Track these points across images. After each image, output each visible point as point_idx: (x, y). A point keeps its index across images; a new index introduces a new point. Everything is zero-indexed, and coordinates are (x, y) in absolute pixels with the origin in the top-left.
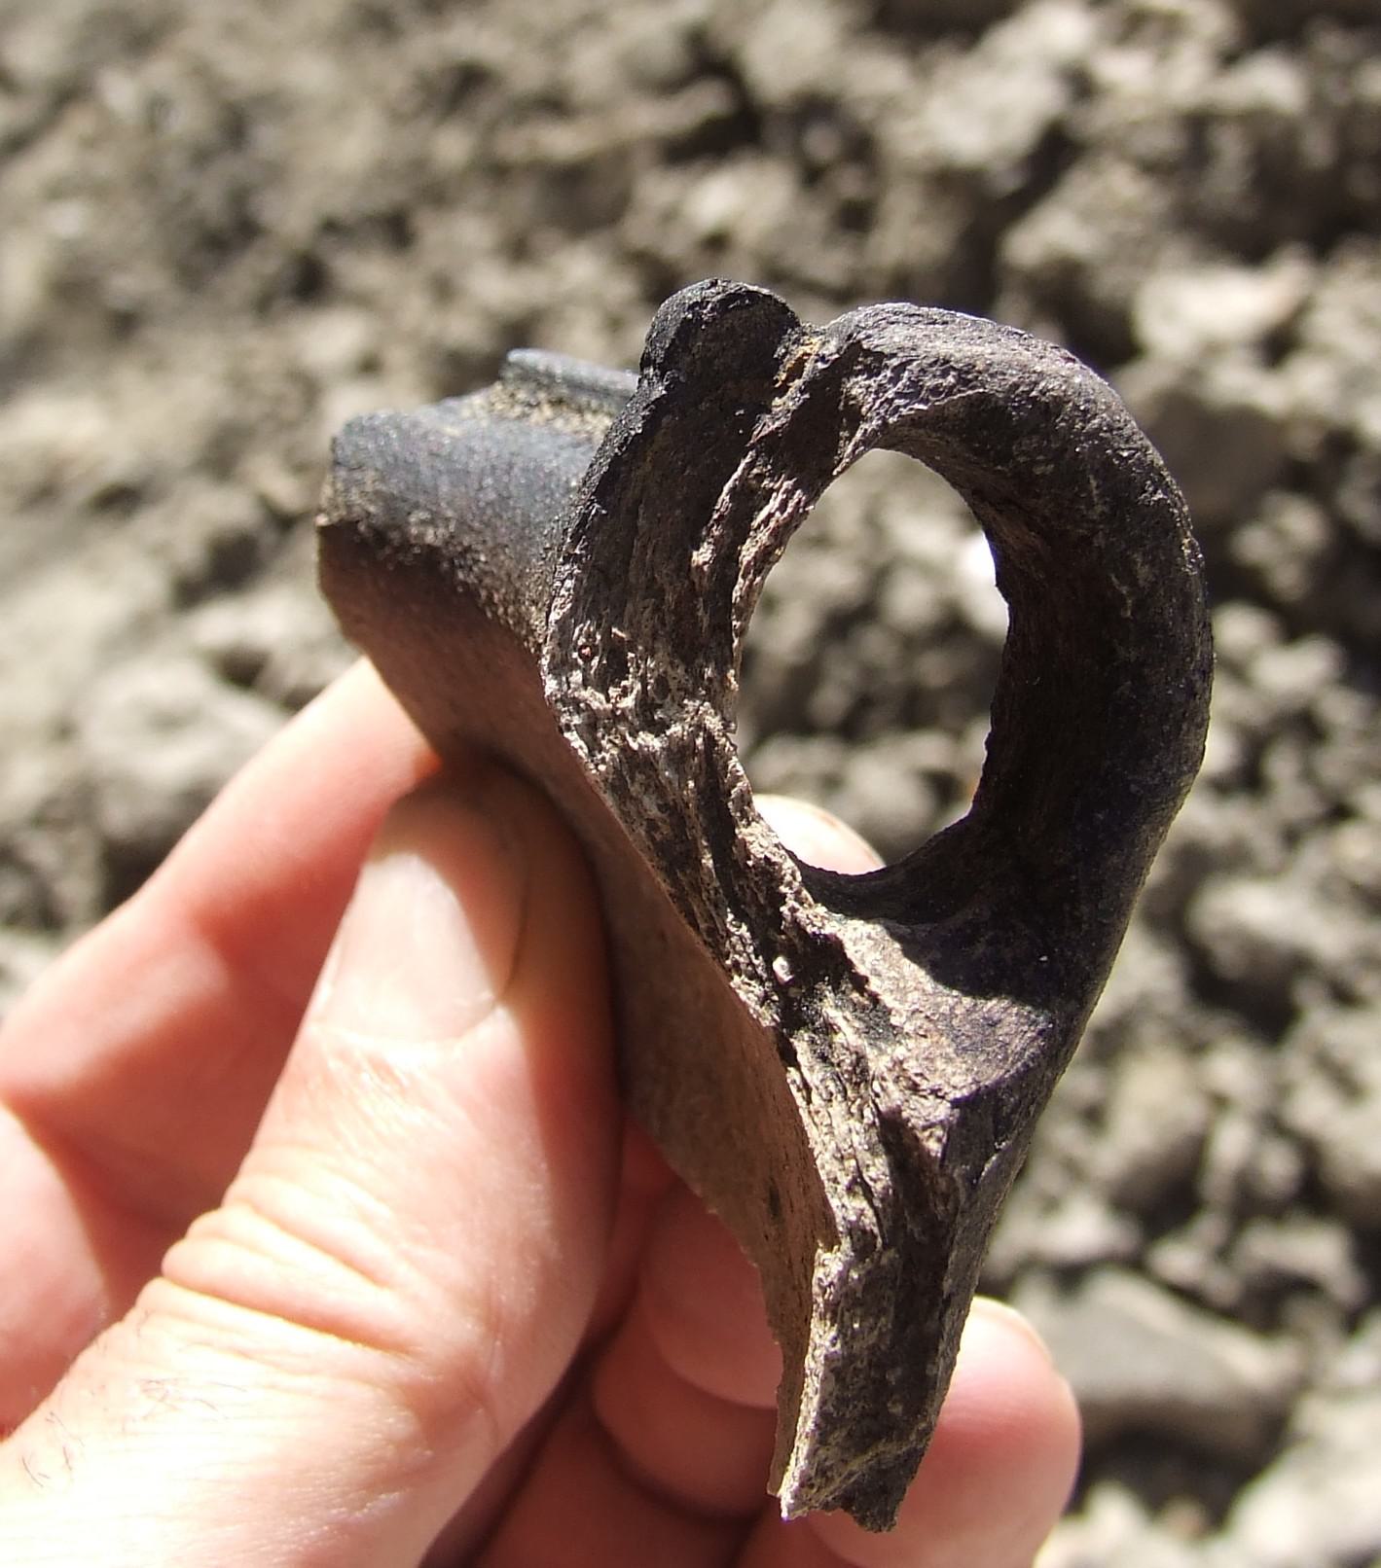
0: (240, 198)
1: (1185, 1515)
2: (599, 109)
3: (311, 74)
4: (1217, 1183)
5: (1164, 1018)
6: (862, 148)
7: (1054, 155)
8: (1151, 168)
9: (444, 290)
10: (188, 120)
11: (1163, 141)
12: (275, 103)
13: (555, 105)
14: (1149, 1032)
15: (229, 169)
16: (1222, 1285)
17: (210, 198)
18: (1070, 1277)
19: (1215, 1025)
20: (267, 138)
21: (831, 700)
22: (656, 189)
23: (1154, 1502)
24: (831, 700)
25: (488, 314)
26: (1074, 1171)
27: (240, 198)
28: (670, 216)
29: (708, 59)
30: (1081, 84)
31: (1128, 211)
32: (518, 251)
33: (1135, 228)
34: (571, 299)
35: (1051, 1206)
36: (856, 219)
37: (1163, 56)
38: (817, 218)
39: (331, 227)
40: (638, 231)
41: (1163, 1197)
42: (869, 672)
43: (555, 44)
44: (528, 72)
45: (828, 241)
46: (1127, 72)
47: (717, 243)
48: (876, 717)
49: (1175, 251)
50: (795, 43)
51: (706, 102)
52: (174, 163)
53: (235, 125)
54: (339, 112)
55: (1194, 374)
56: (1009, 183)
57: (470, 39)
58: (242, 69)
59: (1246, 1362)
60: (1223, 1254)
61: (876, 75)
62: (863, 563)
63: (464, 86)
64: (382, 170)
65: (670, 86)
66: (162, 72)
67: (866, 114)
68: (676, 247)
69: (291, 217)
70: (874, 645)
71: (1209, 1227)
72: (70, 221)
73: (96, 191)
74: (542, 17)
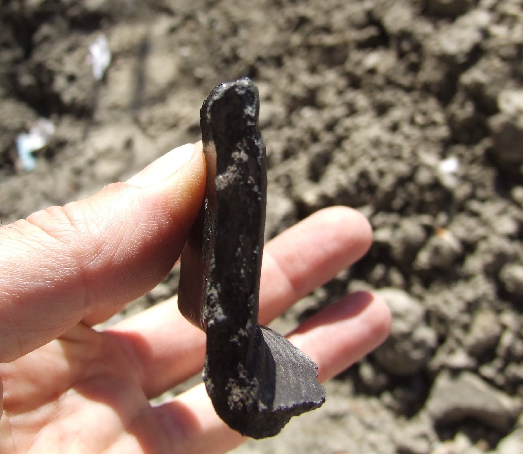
0: (234, 49)
1: (483, 444)
2: (341, 31)
3: (257, 16)
4: (501, 351)
5: (489, 302)
6: (418, 48)
7: (476, 53)
8: (504, 59)
9: (292, 79)
10: (221, 26)
11: (510, 52)
12: (247, 24)
13: (327, 30)
14: (484, 305)
15: (233, 41)
16: (500, 380)
17: (226, 49)
18: (456, 372)
19: (504, 306)
20: (243, 33)
21: (398, 203)
22: (355, 56)
23: (474, 440)
24: (398, 203)
25: (305, 87)
26: (459, 342)
27: (234, 49)
28: (358, 63)
29: (372, 20)
30: (486, 34)
31: (497, 70)
32: (313, 70)
33: (499, 76)
34: (328, 84)
35: (452, 351)
36: (414, 68)
37: (511, 28)
38: (402, 67)
39: (260, 59)
40: (349, 66)
41: (485, 353)
42: (411, 195)
43: (328, 13)
44: (320, 20)
45: (405, 74)
46: (500, 31)
47: (372, 71)
48: (410, 209)
49: (510, 84)
50: (399, 17)
51: (371, 32)
52: (216, 38)
53: (234, 29)
54: (264, 28)
55: (515, 118)
56: (462, 60)
57: (303, 10)
58: (237, 13)
59: (506, 403)
60: (501, 371)
61: (423, 28)
62: (410, 164)
63: (302, 21)
64: (275, 45)
65: (360, 27)
66: (214, 13)
67: (420, 38)
68: (359, 72)
69: (248, 54)
70: (412, 188)
71: (498, 363)
72: (186, 52)
73: (194, 44)
74: (325, 5)
